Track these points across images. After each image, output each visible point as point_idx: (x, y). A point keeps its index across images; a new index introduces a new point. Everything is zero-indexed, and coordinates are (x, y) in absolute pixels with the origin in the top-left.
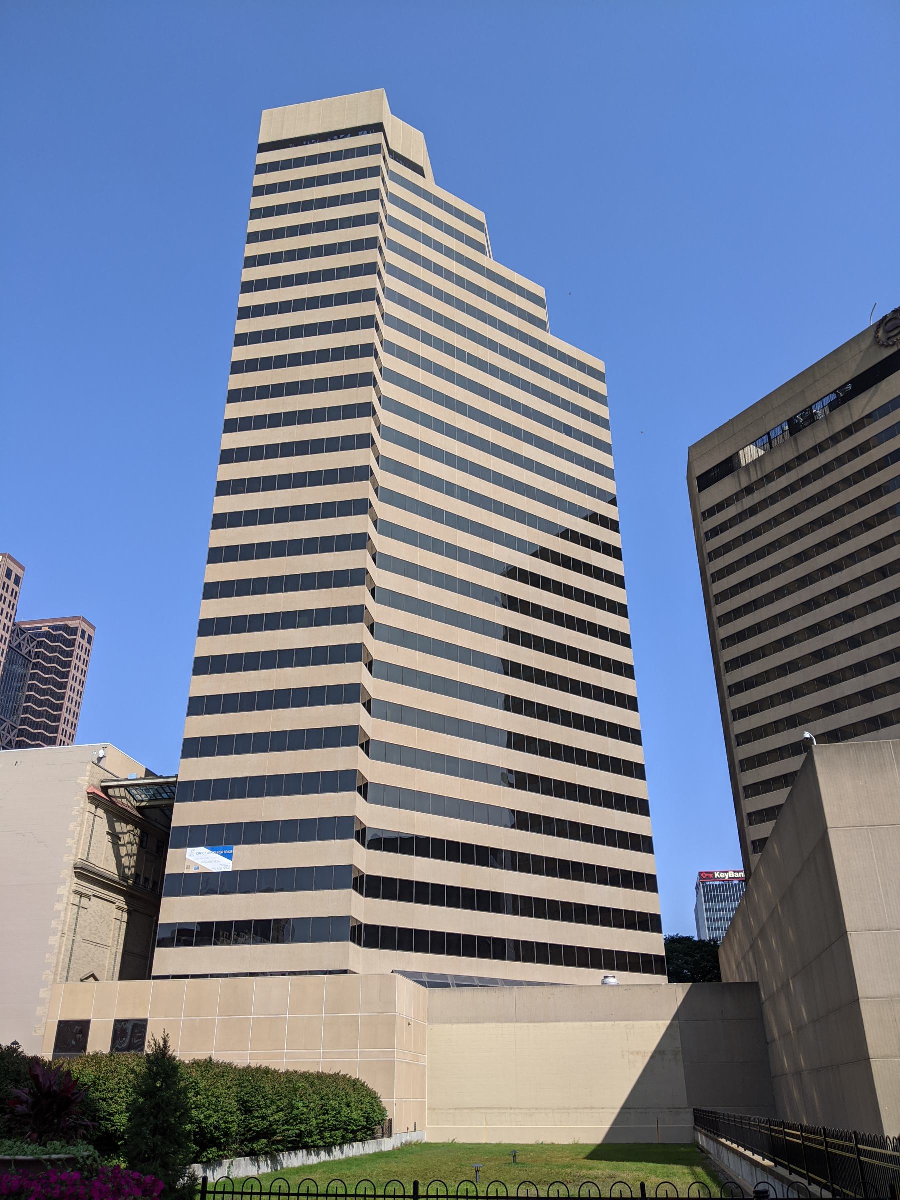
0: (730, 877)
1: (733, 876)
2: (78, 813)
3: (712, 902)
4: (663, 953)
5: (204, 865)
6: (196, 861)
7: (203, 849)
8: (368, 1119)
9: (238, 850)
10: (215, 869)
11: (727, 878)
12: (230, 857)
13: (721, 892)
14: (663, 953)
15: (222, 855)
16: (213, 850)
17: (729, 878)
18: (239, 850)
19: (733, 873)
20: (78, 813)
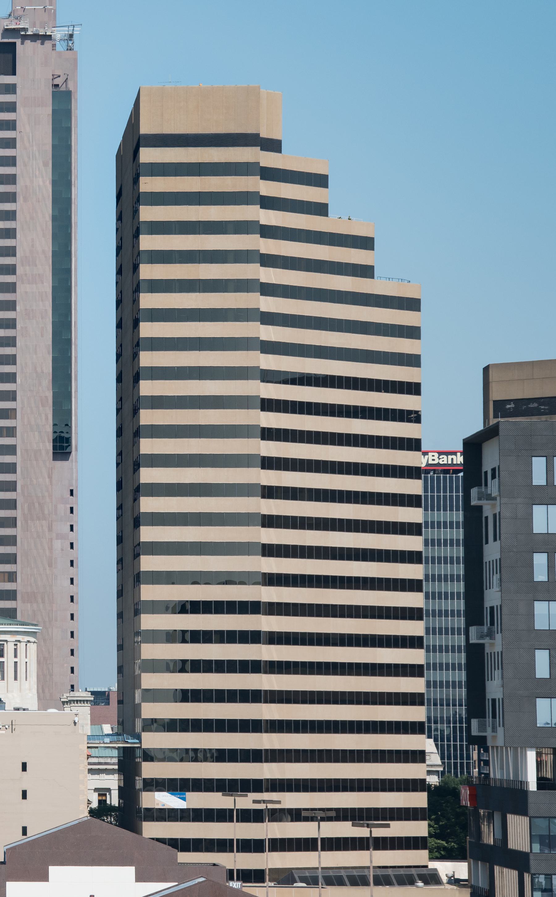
0: (431, 462)
1: (436, 462)
2: (83, 769)
3: (432, 510)
4: (426, 805)
5: (168, 803)
6: (162, 801)
7: (165, 794)
8: (443, 782)
9: (189, 795)
10: (175, 806)
11: (423, 465)
12: (184, 799)
13: (439, 497)
14: (426, 805)
15: (178, 798)
16: (172, 794)
17: (428, 465)
18: (189, 795)
19: (436, 455)
20: (83, 769)
